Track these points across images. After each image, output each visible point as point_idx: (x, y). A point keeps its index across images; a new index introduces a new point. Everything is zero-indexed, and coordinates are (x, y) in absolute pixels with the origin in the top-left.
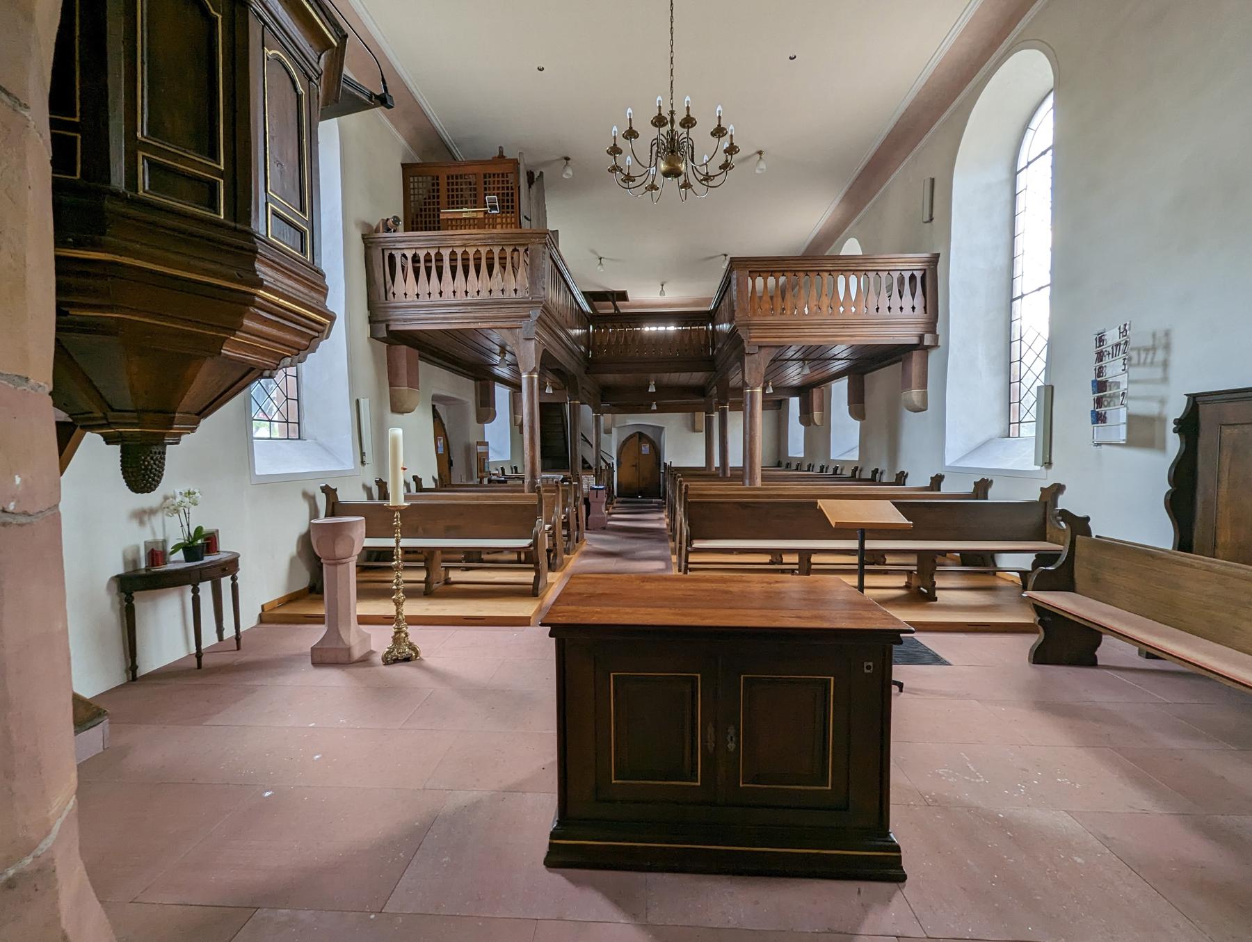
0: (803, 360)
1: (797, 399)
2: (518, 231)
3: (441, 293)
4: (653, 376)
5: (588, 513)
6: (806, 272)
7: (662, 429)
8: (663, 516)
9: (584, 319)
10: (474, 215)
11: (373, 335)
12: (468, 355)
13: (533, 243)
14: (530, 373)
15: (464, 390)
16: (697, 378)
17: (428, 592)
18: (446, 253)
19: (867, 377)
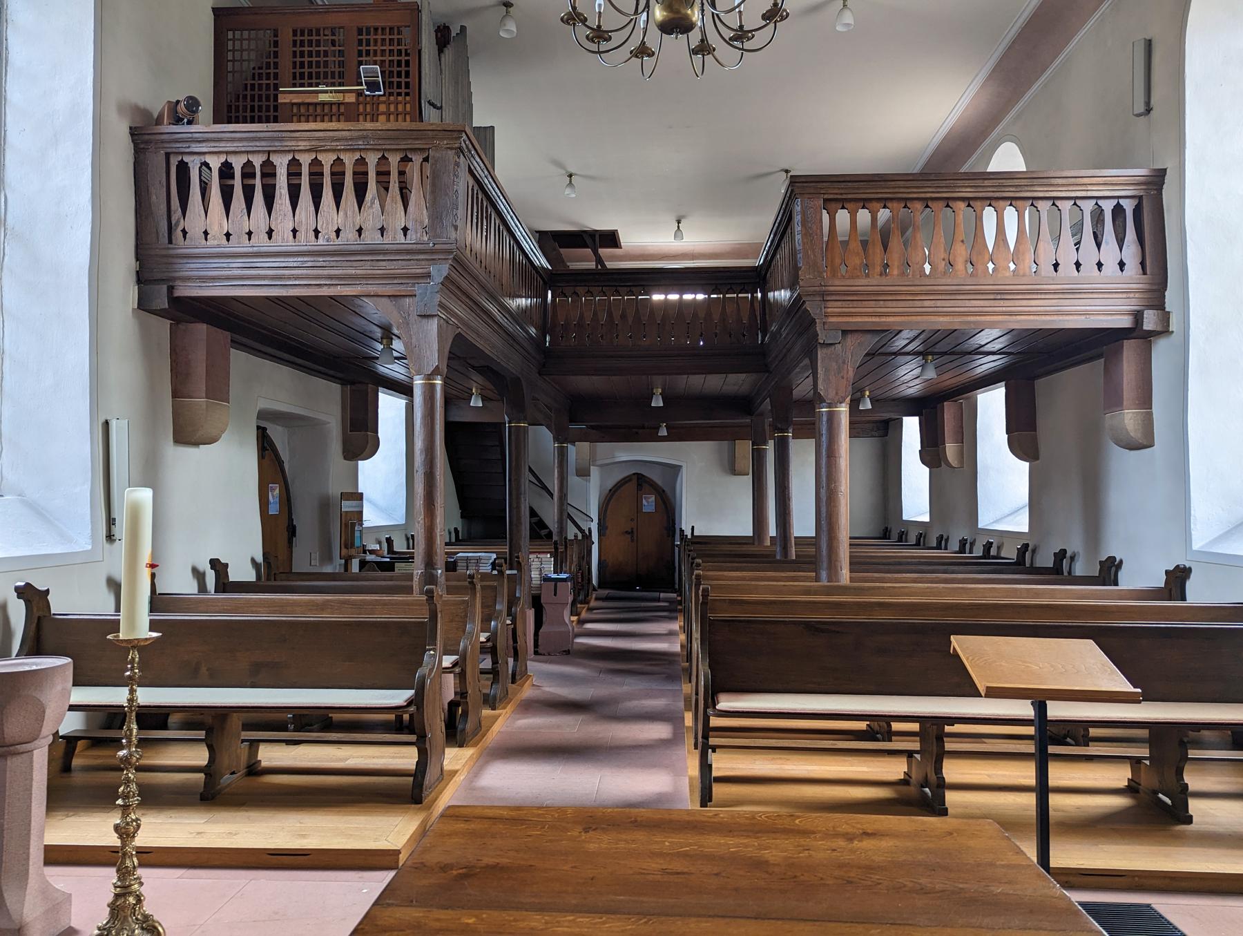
0: (923, 354)
1: (916, 420)
2: (415, 126)
3: (270, 233)
4: (658, 380)
5: (539, 623)
6: (927, 203)
7: (676, 469)
8: (676, 626)
9: (533, 280)
10: (339, 97)
11: (144, 304)
12: (329, 341)
13: (437, 148)
14: (429, 377)
15: (325, 402)
16: (736, 383)
17: (210, 794)
18: (281, 164)
19: (1040, 384)
